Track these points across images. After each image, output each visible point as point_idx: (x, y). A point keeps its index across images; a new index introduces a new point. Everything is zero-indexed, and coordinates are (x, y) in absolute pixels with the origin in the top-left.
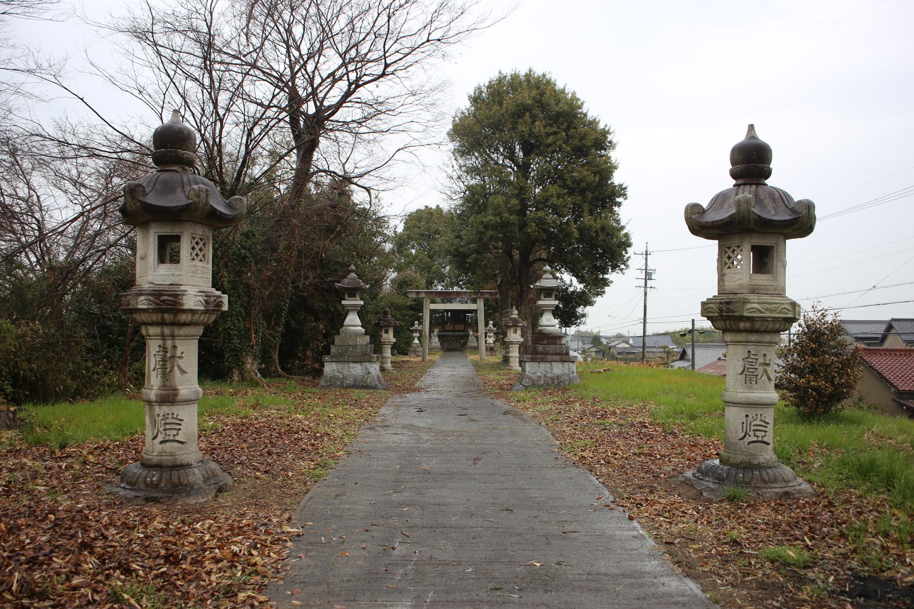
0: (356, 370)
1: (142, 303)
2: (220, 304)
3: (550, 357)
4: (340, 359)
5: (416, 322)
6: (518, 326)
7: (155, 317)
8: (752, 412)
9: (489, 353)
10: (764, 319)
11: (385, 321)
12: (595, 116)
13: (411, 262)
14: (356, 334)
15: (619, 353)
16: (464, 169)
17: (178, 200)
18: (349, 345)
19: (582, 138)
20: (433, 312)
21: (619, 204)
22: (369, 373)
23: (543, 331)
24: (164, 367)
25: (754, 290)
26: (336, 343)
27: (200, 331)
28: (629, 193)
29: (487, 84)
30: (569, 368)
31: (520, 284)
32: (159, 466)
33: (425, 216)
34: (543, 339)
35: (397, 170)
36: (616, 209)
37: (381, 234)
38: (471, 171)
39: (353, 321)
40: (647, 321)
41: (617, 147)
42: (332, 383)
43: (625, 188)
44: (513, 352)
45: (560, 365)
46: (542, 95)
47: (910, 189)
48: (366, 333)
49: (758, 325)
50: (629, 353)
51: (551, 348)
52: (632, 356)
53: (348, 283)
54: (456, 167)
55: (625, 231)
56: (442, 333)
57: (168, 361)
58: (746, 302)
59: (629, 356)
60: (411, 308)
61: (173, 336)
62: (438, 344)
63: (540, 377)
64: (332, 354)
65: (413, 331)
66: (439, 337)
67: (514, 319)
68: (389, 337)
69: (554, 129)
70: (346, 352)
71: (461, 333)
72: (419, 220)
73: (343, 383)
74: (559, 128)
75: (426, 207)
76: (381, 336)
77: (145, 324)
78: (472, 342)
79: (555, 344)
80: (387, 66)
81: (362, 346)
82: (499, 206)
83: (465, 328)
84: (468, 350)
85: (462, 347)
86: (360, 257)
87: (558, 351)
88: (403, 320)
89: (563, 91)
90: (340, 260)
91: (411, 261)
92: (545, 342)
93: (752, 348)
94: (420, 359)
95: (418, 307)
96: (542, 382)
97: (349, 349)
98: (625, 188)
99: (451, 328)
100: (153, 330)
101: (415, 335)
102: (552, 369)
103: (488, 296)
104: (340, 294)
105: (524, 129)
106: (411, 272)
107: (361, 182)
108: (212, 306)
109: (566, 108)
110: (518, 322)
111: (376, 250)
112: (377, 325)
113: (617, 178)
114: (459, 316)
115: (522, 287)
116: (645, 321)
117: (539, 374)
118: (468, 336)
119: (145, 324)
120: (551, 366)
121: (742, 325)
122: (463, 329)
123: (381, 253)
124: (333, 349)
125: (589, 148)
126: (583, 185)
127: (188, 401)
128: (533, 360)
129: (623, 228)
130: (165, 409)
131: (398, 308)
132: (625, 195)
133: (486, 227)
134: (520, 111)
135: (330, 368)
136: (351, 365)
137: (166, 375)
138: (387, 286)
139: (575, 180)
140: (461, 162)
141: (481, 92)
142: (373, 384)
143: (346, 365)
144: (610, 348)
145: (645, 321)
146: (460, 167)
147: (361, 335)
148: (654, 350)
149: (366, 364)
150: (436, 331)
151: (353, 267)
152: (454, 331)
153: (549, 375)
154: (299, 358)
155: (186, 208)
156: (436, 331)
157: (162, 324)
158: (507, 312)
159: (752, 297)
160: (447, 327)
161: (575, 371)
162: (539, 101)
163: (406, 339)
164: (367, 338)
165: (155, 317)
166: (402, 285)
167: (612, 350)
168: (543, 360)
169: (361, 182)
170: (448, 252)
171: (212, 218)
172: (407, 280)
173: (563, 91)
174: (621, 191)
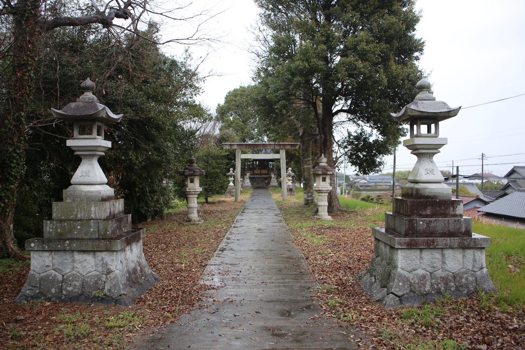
3: (441, 241)
6: (327, 174)
9: (289, 193)
11: (190, 170)
15: (361, 186)
18: (76, 220)
20: (244, 161)
22: (109, 272)
23: (422, 192)
26: (54, 215)
30: (475, 261)
31: (324, 134)
34: (425, 208)
36: (415, 62)
40: (396, 167)
43: (423, 43)
44: (322, 200)
45: (458, 254)
48: (116, 197)
50: (367, 186)
52: (369, 188)
53: (77, 108)
59: (367, 188)
62: (250, 184)
63: (424, 277)
64: (46, 235)
65: (228, 176)
66: (250, 178)
67: (324, 168)
70: (70, 231)
71: (266, 176)
72: (235, 96)
73: (61, 290)
78: (274, 182)
79: (445, 215)
83: (268, 172)
84: (271, 188)
85: (266, 186)
87: (452, 228)
88: (218, 168)
92: (428, 212)
94: (233, 199)
95: (231, 157)
96: (428, 288)
97: (75, 227)
99: (259, 173)
102: (444, 263)
103: (288, 147)
106: (230, 131)
110: (327, 170)
114: (264, 163)
115: (326, 136)
116: (394, 167)
117: (420, 272)
118: (271, 178)
120: (443, 255)
122: (267, 172)
124: (48, 227)
126: (392, 32)
128: (411, 246)
136: (78, 256)
139: (382, 28)
142: (115, 293)
143: (68, 256)
144: (355, 183)
145: (394, 167)
148: (382, 184)
149: (103, 255)
150: (248, 175)
152: (261, 174)
153: (439, 273)
156: (248, 175)
160: (256, 172)
161: (484, 265)
163: (221, 183)
164: (119, 205)
167: (357, 184)
168: (430, 246)
170: (256, 101)
172: (225, 137)
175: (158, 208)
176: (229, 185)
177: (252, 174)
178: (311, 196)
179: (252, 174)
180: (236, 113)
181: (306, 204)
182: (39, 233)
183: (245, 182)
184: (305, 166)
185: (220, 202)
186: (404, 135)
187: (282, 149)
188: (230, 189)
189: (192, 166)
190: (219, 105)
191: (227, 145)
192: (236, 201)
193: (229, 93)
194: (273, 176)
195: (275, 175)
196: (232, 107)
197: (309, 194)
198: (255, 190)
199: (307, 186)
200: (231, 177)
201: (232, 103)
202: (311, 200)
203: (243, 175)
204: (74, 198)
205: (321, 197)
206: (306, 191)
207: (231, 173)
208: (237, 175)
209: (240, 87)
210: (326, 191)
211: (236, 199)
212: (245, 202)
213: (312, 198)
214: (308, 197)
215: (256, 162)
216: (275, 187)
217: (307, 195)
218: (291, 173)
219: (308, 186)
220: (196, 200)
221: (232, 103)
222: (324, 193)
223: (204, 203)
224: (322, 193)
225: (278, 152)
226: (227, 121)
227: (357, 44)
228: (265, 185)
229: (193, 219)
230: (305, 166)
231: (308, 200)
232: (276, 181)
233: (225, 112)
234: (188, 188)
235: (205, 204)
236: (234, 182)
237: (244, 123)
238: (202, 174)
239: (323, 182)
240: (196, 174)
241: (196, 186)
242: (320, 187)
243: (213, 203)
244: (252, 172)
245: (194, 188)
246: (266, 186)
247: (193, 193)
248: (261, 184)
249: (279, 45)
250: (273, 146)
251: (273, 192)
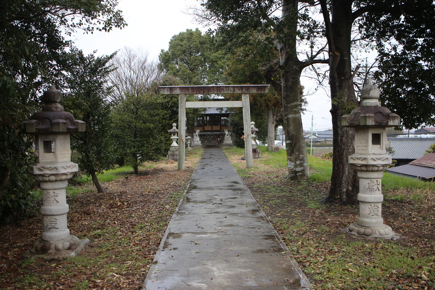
5: (174, 124)
44: (370, 190)
50: (317, 142)
52: (319, 144)
56: (202, 133)
59: (317, 144)
60: (164, 106)
65: (171, 134)
66: (200, 136)
71: (218, 133)
72: (181, 40)
75: (187, 30)
76: (36, 160)
84: (225, 147)
85: (218, 144)
88: (152, 122)
94: (176, 164)
99: (210, 129)
101: (173, 137)
122: (219, 129)
150: (198, 132)
152: (212, 131)
156: (198, 132)
158: (296, 106)
160: (207, 128)
175: (11, 201)
176: (172, 145)
177: (202, 130)
178: (301, 165)
179: (202, 130)
180: (182, 60)
181: (292, 178)
183: (194, 140)
184: (290, 116)
185: (156, 171)
187: (245, 94)
188: (173, 151)
189: (50, 110)
190: (162, 51)
191: (166, 89)
192: (179, 169)
193: (174, 37)
194: (227, 133)
195: (229, 131)
196: (178, 53)
197: (298, 162)
198: (206, 149)
199: (293, 149)
200: (174, 135)
201: (177, 48)
202: (301, 172)
203: (190, 131)
205: (368, 181)
206: (292, 157)
207: (174, 130)
208: (180, 132)
210: (381, 168)
211: (179, 165)
212: (192, 172)
213: (302, 168)
214: (296, 166)
215: (207, 118)
216: (230, 145)
217: (293, 164)
218: (254, 128)
219: (296, 148)
220: (62, 196)
221: (177, 48)
222: (377, 171)
223: (131, 173)
224: (372, 171)
225: (238, 98)
226: (172, 69)
228: (217, 144)
229: (54, 243)
230: (290, 116)
231: (296, 172)
232: (230, 139)
233: (169, 58)
234: (39, 166)
235: (133, 178)
237: (192, 71)
238: (76, 130)
239: (375, 146)
240: (55, 130)
241: (60, 160)
242: (369, 157)
243: (146, 173)
244: (202, 128)
245: (53, 166)
246: (218, 144)
247: (53, 178)
248: (213, 143)
250: (232, 89)
251: (228, 152)
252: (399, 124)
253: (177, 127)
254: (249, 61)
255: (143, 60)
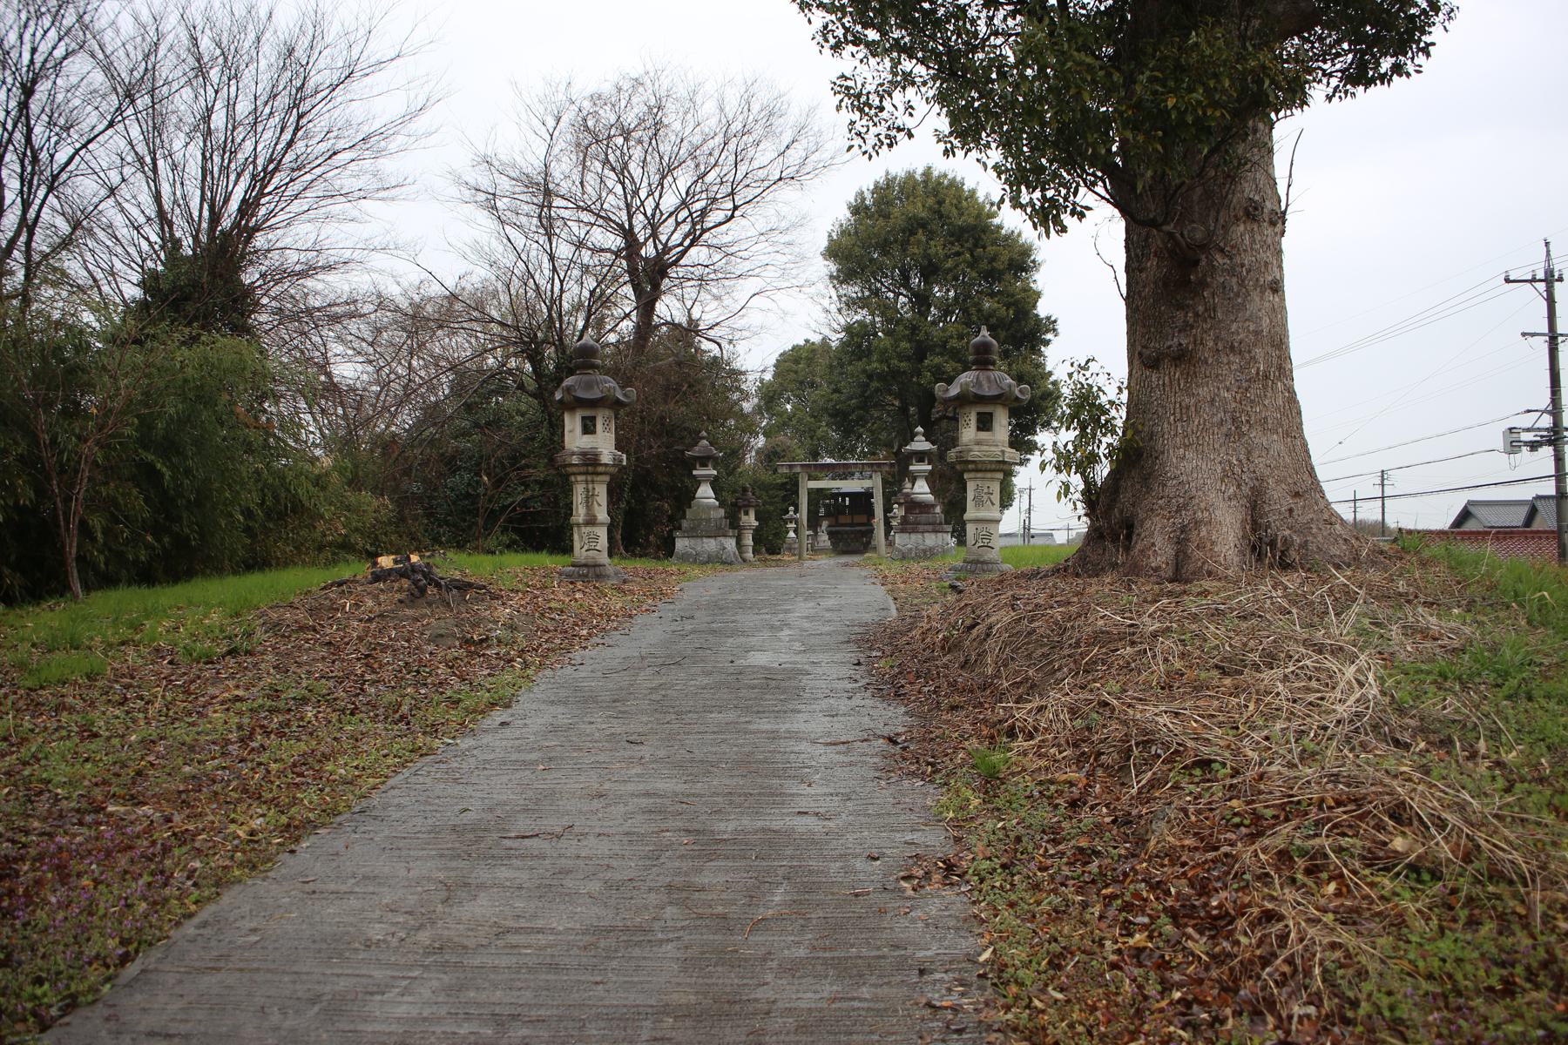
0: (711, 545)
1: (575, 460)
2: (621, 461)
3: (921, 528)
4: (693, 533)
5: (792, 508)
7: (582, 469)
8: (980, 526)
10: (983, 462)
12: (1012, 228)
13: (784, 424)
14: (709, 507)
16: (844, 299)
17: (595, 394)
19: (993, 259)
21: (1047, 343)
24: (587, 502)
25: (978, 443)
27: (607, 478)
28: (1060, 326)
29: (872, 187)
32: (586, 565)
33: (804, 355)
35: (753, 318)
37: (738, 389)
38: (851, 304)
39: (705, 492)
41: (1042, 269)
42: (685, 558)
43: (1055, 321)
45: (933, 536)
46: (940, 203)
47: (1428, 314)
49: (980, 466)
51: (923, 517)
53: (699, 451)
54: (835, 298)
55: (1052, 379)
56: (834, 529)
57: (589, 498)
58: (971, 450)
61: (593, 482)
68: (750, 520)
69: (957, 248)
71: (863, 528)
72: (797, 361)
74: (962, 246)
77: (574, 474)
80: (736, 208)
81: (716, 520)
82: (886, 350)
86: (712, 421)
88: (771, 504)
89: (973, 192)
90: (687, 425)
91: (785, 422)
93: (979, 483)
98: (1055, 321)
99: (849, 521)
100: (580, 478)
101: (789, 525)
104: (690, 464)
105: (916, 251)
106: (785, 439)
107: (711, 333)
108: (617, 461)
109: (971, 221)
111: (733, 410)
112: (734, 505)
113: (1043, 310)
119: (574, 474)
121: (970, 466)
123: (741, 415)
124: (685, 524)
125: (1001, 273)
127: (602, 524)
129: (1050, 374)
130: (589, 529)
131: (765, 487)
132: (1054, 330)
133: (870, 377)
134: (914, 225)
135: (681, 544)
136: (705, 540)
137: (589, 507)
138: (750, 459)
140: (842, 292)
141: (864, 199)
146: (839, 297)
147: (714, 508)
149: (722, 539)
150: (825, 524)
151: (704, 433)
152: (852, 525)
153: (921, 547)
154: (640, 545)
155: (602, 398)
156: (825, 524)
157: (586, 473)
159: (976, 448)
160: (842, 519)
162: (939, 212)
164: (722, 512)
165: (582, 469)
166: (770, 456)
168: (914, 531)
169: (711, 333)
171: (616, 405)
172: (779, 449)
173: (973, 192)
174: (1050, 325)
182: (680, 528)
186: (1109, 445)
203: (814, 523)
204: (699, 506)
209: (807, 341)
215: (844, 500)
226: (780, 415)
227: (946, 342)
236: (796, 531)
237: (815, 417)
249: (852, 337)
252: (602, 482)
253: (796, 511)
254: (922, 62)
255: (332, 256)
